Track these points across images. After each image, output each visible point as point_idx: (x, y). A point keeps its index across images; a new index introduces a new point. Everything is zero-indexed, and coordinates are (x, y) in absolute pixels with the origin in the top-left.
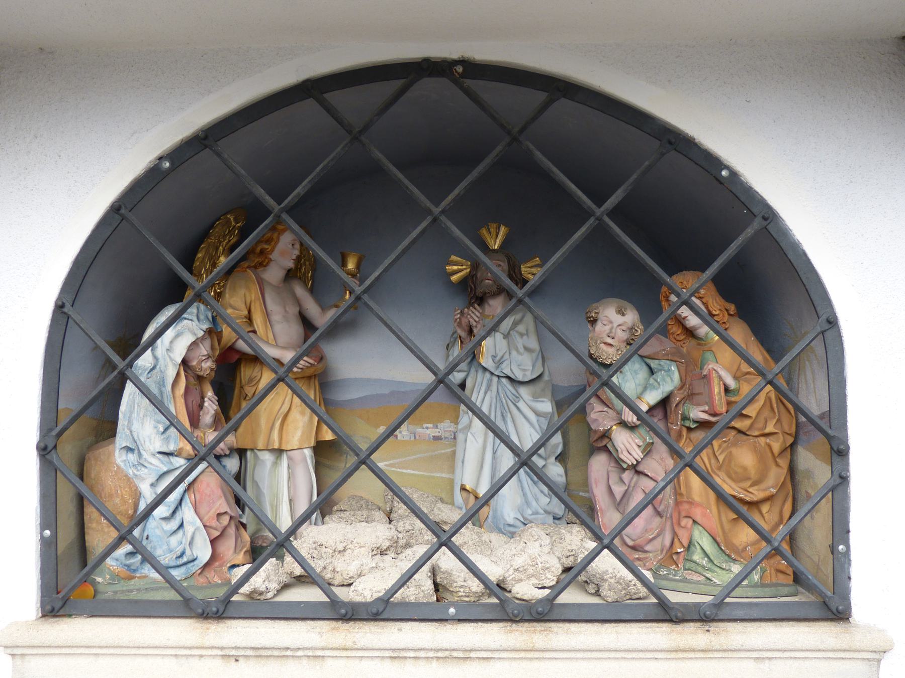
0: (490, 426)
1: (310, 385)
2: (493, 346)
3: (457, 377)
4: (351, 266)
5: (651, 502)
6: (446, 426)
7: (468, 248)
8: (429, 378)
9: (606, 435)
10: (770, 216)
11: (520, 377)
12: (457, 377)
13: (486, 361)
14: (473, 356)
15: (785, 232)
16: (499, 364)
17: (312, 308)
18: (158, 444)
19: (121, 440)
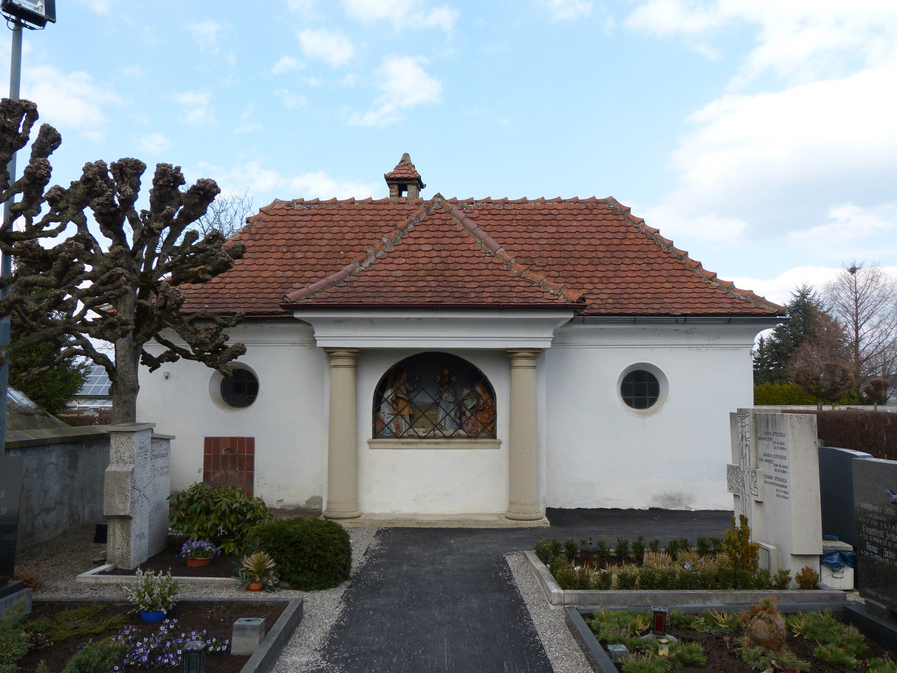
0: (444, 410)
1: (836, 320)
2: (445, 395)
3: (438, 401)
4: (417, 379)
5: (439, 230)
6: (435, 412)
7: (878, 607)
8: (433, 402)
9: (465, 412)
10: (486, 377)
11: (450, 401)
12: (438, 401)
13: (443, 398)
14: (441, 397)
15: (488, 380)
16: (446, 398)
17: (408, 387)
18: (388, 412)
19: (382, 412)
